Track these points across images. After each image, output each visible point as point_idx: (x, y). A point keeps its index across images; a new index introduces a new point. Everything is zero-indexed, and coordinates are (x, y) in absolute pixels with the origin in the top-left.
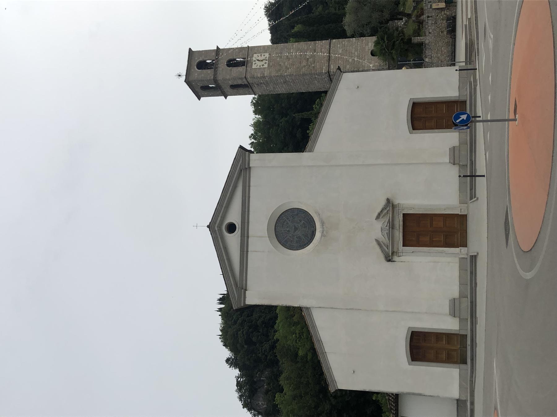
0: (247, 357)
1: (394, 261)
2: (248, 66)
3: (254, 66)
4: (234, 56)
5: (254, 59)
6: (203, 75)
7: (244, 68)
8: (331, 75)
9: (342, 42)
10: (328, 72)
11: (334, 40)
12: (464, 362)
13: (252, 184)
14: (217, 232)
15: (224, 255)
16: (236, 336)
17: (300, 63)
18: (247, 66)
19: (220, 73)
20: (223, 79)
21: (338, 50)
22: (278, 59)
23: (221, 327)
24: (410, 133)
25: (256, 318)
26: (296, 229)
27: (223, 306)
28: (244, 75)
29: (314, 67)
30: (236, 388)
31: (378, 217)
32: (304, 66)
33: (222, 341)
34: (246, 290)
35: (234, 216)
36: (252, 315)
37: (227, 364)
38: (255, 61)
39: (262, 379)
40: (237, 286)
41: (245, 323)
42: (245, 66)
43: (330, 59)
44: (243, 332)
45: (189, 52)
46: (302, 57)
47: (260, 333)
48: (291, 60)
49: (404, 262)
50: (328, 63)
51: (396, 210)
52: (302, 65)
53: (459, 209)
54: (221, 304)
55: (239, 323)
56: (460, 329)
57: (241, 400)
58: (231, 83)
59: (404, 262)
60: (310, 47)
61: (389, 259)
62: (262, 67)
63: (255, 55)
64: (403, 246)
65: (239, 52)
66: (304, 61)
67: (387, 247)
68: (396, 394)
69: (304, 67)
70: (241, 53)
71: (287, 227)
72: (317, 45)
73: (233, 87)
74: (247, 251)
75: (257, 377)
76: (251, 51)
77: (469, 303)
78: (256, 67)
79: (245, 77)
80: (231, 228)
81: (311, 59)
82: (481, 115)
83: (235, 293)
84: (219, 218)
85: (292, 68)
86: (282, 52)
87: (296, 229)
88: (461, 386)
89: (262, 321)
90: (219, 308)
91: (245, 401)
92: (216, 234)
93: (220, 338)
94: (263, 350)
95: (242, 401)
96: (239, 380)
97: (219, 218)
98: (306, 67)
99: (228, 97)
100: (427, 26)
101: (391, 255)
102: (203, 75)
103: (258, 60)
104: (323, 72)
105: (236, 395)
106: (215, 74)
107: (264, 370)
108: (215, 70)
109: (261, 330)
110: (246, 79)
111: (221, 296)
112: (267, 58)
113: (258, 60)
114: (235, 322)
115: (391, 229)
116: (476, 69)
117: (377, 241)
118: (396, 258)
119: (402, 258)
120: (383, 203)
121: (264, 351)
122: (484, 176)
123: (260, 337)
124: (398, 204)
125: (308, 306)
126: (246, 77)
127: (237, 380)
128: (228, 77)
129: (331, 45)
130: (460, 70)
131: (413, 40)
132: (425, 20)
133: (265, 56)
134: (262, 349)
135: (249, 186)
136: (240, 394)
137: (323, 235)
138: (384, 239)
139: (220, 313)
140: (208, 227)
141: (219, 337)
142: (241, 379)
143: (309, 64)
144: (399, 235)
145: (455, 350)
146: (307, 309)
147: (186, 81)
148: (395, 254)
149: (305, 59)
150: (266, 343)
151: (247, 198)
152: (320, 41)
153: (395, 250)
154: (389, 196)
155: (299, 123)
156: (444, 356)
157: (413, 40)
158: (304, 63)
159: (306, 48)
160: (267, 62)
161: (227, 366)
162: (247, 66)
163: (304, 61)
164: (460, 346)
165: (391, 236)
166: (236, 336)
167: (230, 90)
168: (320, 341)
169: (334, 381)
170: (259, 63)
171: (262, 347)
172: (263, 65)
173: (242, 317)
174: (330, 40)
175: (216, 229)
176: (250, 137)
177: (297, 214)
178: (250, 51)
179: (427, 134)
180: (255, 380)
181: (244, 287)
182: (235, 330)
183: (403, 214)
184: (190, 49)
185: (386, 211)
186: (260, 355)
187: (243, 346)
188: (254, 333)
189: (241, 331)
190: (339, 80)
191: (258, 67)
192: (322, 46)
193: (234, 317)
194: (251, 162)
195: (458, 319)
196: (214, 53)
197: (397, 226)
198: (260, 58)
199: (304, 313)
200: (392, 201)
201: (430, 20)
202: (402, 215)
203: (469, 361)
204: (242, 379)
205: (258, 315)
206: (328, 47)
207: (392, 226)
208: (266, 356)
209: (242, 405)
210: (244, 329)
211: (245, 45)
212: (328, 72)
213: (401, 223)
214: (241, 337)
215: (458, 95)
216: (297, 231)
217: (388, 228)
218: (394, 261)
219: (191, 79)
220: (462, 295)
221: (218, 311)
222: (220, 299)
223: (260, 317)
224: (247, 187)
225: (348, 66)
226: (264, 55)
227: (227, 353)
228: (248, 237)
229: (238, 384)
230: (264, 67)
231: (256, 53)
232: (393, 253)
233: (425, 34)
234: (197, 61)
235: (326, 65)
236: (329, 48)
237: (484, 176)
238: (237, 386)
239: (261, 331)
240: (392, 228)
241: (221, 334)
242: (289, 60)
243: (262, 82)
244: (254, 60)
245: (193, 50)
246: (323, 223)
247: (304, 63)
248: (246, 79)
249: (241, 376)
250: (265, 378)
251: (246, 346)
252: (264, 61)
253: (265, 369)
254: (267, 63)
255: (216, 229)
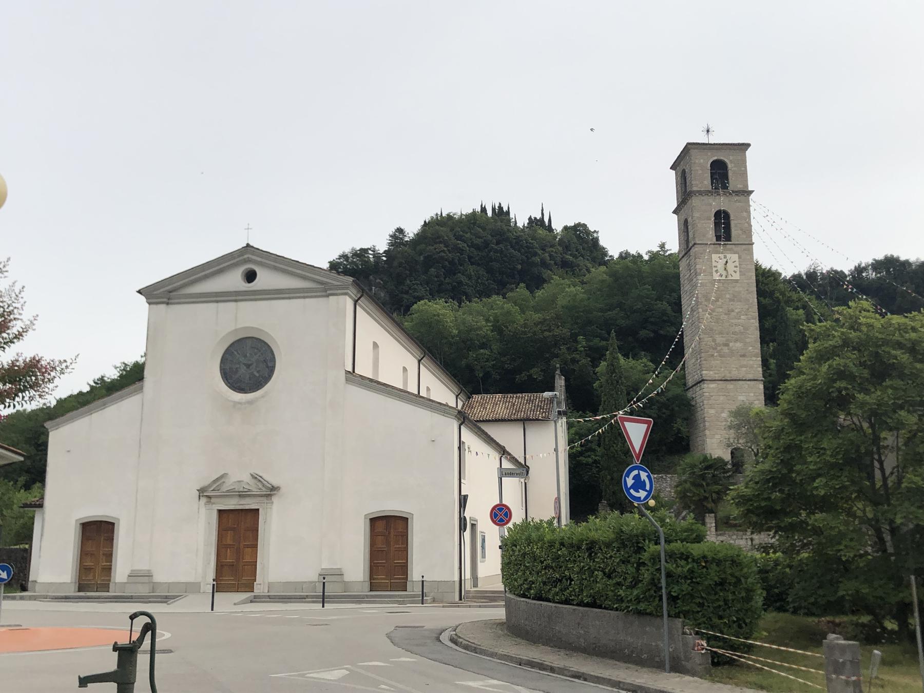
0: (404, 261)
1: (199, 499)
2: (716, 246)
3: (715, 257)
4: (736, 222)
5: (728, 256)
6: (700, 172)
7: (712, 241)
8: (701, 384)
9: (758, 400)
10: (703, 380)
11: (761, 386)
12: (80, 589)
13: (307, 300)
14: (241, 258)
15: (211, 270)
16: (437, 240)
17: (721, 333)
18: (716, 244)
19: (703, 200)
20: (693, 206)
21: (743, 394)
22: (728, 296)
23: (454, 214)
24: (365, 515)
25: (467, 271)
26: (248, 366)
27: (490, 213)
28: (698, 242)
29: (713, 355)
30: (358, 249)
31: (254, 477)
32: (714, 340)
33: (432, 218)
34: (168, 304)
35: (266, 279)
36: (472, 264)
37: (394, 231)
38: (725, 257)
39: (373, 288)
40: (170, 292)
41: (459, 254)
42: (717, 241)
43: (728, 382)
44: (443, 251)
45: (743, 144)
46: (732, 335)
47: (443, 280)
48: (726, 317)
49: (198, 512)
50: (720, 378)
51: (264, 499)
52: (717, 336)
53: (262, 582)
54: (494, 209)
55: (458, 244)
56: (116, 583)
57: (341, 256)
58: (689, 220)
59: (198, 512)
60: (750, 348)
61: (202, 491)
62: (714, 269)
63: (735, 257)
64: (220, 511)
65: (742, 230)
66: (724, 339)
67: (216, 489)
68: (43, 504)
69: (713, 340)
70: (740, 232)
71: (251, 354)
72: (754, 359)
73: (686, 222)
74: (217, 302)
75: (376, 279)
76: (744, 250)
77: (130, 594)
78: (713, 261)
79: (695, 244)
80: (250, 276)
81: (727, 351)
82: (325, 608)
83: (162, 290)
84: (259, 259)
85: (711, 320)
86: (741, 302)
87: (248, 366)
88: (51, 584)
89: (462, 281)
90: (486, 207)
91: (338, 263)
92: (239, 256)
93: (437, 214)
94: (416, 287)
95: (339, 259)
96: (370, 252)
97: (259, 259)
98: (713, 343)
99: (675, 216)
100: (734, 537)
101: (205, 494)
102: (700, 172)
103: (727, 262)
104: (704, 372)
105: (347, 250)
106: (700, 193)
107: (386, 290)
108: (710, 192)
109: (448, 281)
110: (693, 246)
111: (505, 209)
112: (730, 278)
113: (727, 262)
114: (459, 238)
115: (237, 493)
116: (423, 604)
117: (224, 476)
118: (204, 500)
119: (203, 510)
120: (275, 483)
121: (415, 289)
122: (212, 610)
123: (436, 279)
124: (272, 503)
125: (145, 389)
126: (696, 246)
127: (370, 249)
128: (696, 215)
129: (753, 383)
130: (423, 581)
131: (709, 516)
132: (746, 534)
133: (733, 274)
134: (417, 284)
135: (304, 297)
136: (350, 255)
137: (236, 404)
138: (228, 485)
139: (479, 209)
140: (248, 245)
141: (439, 213)
142: (370, 254)
143: (719, 348)
144: (232, 504)
145: (94, 576)
146: (141, 388)
147: (689, 146)
148: (208, 500)
149: (728, 340)
150: (426, 290)
151: (287, 296)
152: (760, 363)
153: (213, 500)
154: (283, 490)
155: (662, 332)
156: (88, 563)
157: (709, 516)
158: (719, 339)
159: (748, 340)
160: (724, 278)
161: (391, 230)
162: (716, 244)
163: (724, 339)
164: (100, 584)
165: (229, 494)
166: (437, 240)
167: (683, 218)
168: (104, 406)
169: (57, 426)
170: (720, 266)
171: (421, 284)
172: (717, 271)
173: (468, 248)
174: (762, 380)
175: (246, 256)
176: (649, 252)
177: (267, 367)
178: (744, 247)
179: (363, 537)
180: (371, 277)
181: (170, 301)
182: (446, 238)
183: (258, 510)
184: (748, 145)
185: (261, 486)
186: (408, 282)
187: (421, 254)
188: (443, 270)
189: (445, 249)
190: (445, 414)
191: (714, 264)
192: (752, 367)
193: (468, 235)
194: (335, 297)
195: (125, 581)
196: (741, 186)
197: (243, 501)
198: (730, 267)
199: (138, 384)
200: (274, 494)
201: (747, 543)
202: (256, 508)
203: (82, 594)
204: (371, 256)
205: (473, 274)
206: (751, 376)
207: (242, 495)
208: (407, 293)
209: (334, 260)
210: (448, 253)
211: (755, 239)
212: (703, 380)
213: (247, 507)
214: (435, 249)
215: (414, 580)
216: (245, 368)
217: (241, 489)
218: (199, 499)
219: (693, 152)
220: (155, 586)
221: (482, 205)
222: (500, 208)
223: (470, 278)
224: (302, 295)
225: (712, 411)
226: (735, 272)
227: (412, 229)
228: (236, 301)
229: (364, 251)
230: (714, 273)
231: (740, 257)
232: (209, 497)
233: (721, 535)
234: (726, 160)
235: (716, 375)
236: (748, 379)
237: (212, 610)
238: (361, 250)
239: (447, 280)
240: (240, 495)
241: (444, 215)
242: (726, 314)
243: (692, 272)
244: (727, 255)
245: (749, 153)
246: (250, 403)
247: (719, 339)
248: (693, 246)
249: (377, 256)
250: (375, 294)
251: (422, 258)
252: (724, 273)
253: (387, 292)
254: (721, 278)
255: (246, 256)
